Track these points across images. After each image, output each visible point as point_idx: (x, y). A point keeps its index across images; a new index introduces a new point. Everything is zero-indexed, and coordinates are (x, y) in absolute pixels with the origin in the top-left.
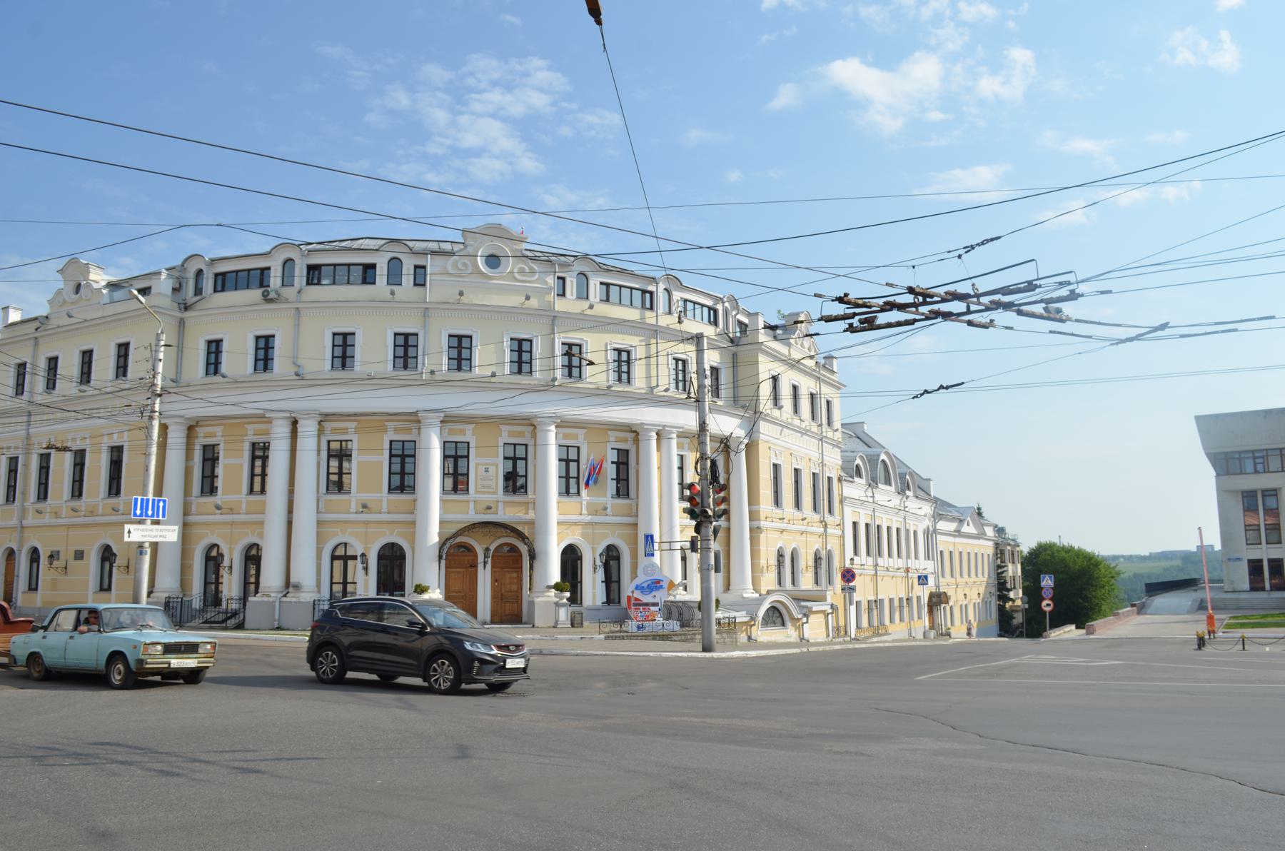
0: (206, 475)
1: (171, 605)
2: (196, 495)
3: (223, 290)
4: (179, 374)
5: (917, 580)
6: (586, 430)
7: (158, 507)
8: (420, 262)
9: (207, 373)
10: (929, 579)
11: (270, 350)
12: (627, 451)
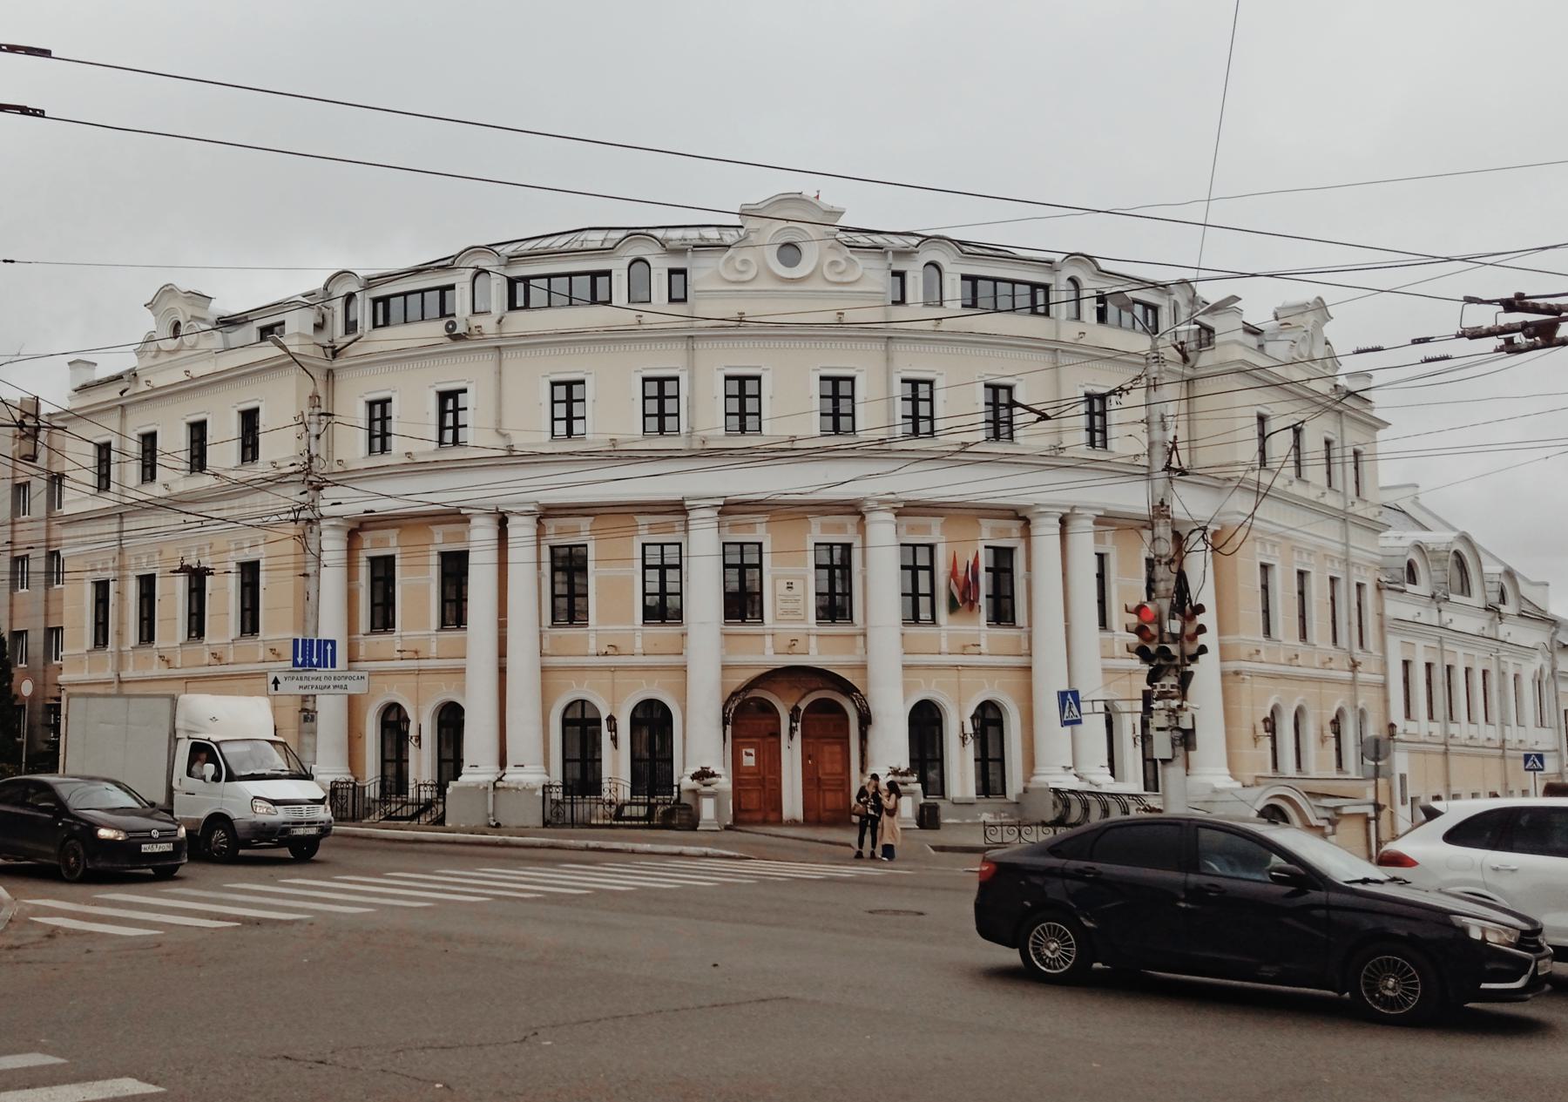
0: (376, 601)
1: (339, 792)
2: (364, 632)
3: (386, 323)
4: (330, 454)
5: (1522, 762)
6: (943, 519)
7: (325, 651)
8: (677, 263)
9: (371, 451)
10: (1546, 761)
11: (388, 422)
12: (1010, 551)
